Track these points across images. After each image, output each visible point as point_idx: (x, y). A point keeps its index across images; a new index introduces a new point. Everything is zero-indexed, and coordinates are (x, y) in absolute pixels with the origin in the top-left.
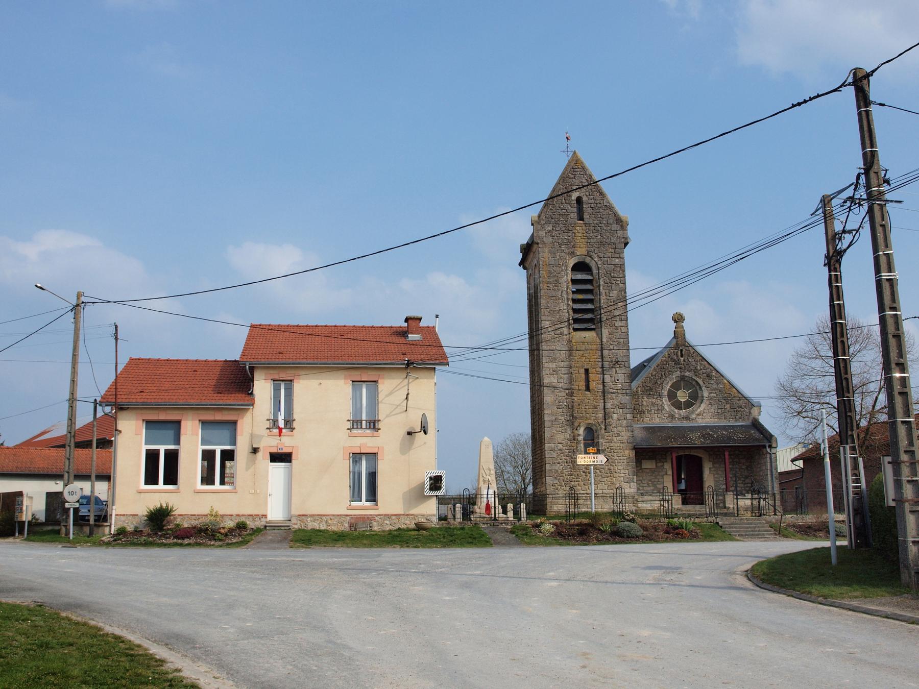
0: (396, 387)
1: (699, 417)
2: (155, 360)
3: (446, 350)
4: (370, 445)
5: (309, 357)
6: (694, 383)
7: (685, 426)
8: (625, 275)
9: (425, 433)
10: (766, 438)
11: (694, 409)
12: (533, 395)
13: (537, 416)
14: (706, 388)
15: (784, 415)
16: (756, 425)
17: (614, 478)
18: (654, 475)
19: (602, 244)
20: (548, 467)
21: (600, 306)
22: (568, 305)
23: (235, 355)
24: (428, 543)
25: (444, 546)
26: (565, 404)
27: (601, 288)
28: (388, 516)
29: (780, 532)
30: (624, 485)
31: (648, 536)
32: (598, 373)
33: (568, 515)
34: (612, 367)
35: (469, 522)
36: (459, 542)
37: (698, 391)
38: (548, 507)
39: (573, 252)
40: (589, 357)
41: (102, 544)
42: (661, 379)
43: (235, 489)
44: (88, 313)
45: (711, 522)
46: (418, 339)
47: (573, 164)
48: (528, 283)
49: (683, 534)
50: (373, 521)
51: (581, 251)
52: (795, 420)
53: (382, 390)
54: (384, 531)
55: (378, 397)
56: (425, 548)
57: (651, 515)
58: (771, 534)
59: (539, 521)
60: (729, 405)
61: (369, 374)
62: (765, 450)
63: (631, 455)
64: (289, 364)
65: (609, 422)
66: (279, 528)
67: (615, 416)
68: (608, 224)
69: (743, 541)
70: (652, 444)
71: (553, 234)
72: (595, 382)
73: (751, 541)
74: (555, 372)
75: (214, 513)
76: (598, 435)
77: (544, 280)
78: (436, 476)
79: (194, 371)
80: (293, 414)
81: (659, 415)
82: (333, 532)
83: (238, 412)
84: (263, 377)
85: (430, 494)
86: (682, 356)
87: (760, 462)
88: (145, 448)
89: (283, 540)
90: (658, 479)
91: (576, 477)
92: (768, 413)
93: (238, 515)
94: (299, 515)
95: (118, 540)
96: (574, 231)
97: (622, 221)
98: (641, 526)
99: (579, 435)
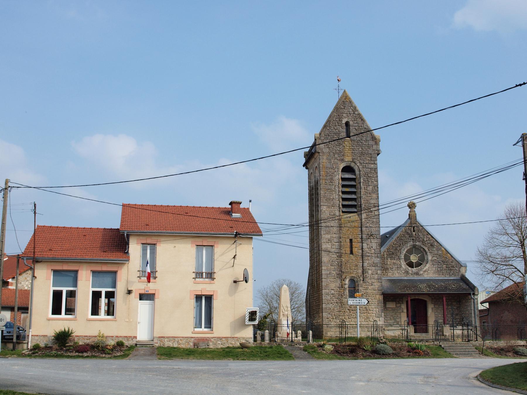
0: (226, 250)
1: (425, 273)
2: (55, 227)
3: (259, 225)
4: (208, 289)
5: (167, 229)
6: (422, 250)
7: (416, 279)
8: (378, 175)
9: (246, 282)
10: (471, 288)
11: (422, 268)
12: (312, 256)
13: (316, 271)
14: (430, 254)
15: (481, 272)
16: (464, 279)
17: (369, 314)
18: (394, 312)
19: (362, 154)
20: (324, 306)
21: (361, 196)
22: (339, 195)
23: (116, 224)
24: (251, 357)
25: (262, 359)
26: (336, 263)
27: (362, 184)
28: (220, 338)
29: (483, 352)
30: (377, 319)
31: (396, 354)
32: (359, 242)
33: (341, 339)
34: (368, 239)
35: (275, 343)
36: (272, 357)
37: (425, 255)
38: (324, 333)
39: (343, 159)
40: (353, 231)
41: (24, 356)
42: (400, 246)
43: (115, 318)
44: (13, 194)
45: (436, 345)
46: (239, 217)
47: (343, 99)
48: (309, 178)
49: (419, 353)
50: (209, 342)
51: (348, 159)
52: (489, 276)
53: (217, 252)
54: (218, 349)
55: (214, 257)
56: (250, 360)
57: (394, 340)
58: (477, 354)
59: (322, 343)
60: (445, 266)
61: (208, 240)
62: (470, 296)
63: (380, 298)
64: (154, 233)
65: (366, 276)
66: (146, 346)
67: (370, 272)
68: (366, 141)
69: (459, 358)
70: (394, 291)
71: (330, 146)
72: (356, 248)
73: (464, 358)
74: (330, 240)
75: (101, 335)
76: (358, 285)
77: (323, 178)
78: (252, 311)
79: (84, 236)
80: (156, 267)
81: (398, 271)
82: (184, 349)
83: (118, 265)
84: (136, 241)
85: (249, 324)
86: (414, 231)
87: (466, 304)
88: (52, 289)
89: (152, 354)
90: (398, 315)
91: (343, 313)
92: (470, 271)
93: (117, 337)
94: (159, 337)
95: (36, 353)
96: (343, 145)
97: (376, 139)
98: (391, 347)
99: (345, 284)
